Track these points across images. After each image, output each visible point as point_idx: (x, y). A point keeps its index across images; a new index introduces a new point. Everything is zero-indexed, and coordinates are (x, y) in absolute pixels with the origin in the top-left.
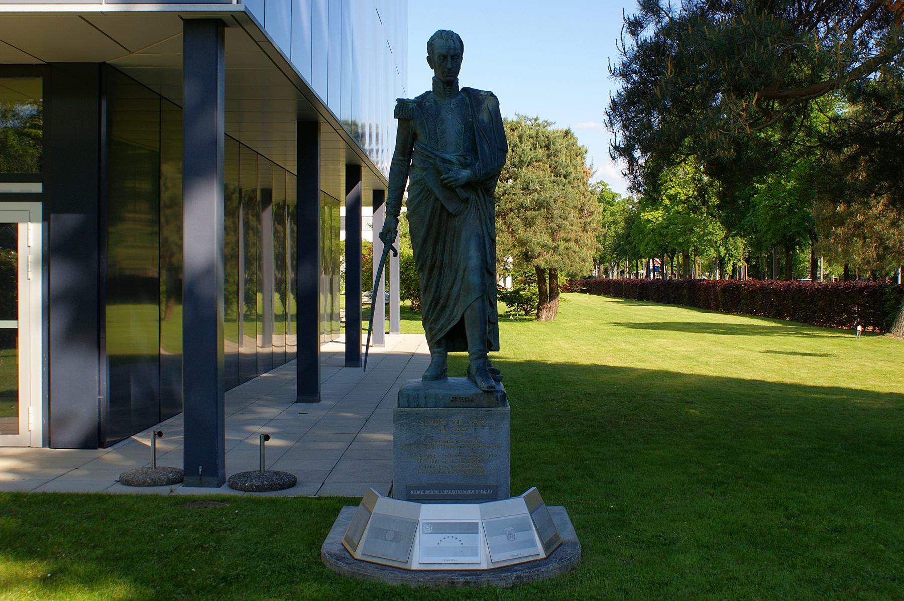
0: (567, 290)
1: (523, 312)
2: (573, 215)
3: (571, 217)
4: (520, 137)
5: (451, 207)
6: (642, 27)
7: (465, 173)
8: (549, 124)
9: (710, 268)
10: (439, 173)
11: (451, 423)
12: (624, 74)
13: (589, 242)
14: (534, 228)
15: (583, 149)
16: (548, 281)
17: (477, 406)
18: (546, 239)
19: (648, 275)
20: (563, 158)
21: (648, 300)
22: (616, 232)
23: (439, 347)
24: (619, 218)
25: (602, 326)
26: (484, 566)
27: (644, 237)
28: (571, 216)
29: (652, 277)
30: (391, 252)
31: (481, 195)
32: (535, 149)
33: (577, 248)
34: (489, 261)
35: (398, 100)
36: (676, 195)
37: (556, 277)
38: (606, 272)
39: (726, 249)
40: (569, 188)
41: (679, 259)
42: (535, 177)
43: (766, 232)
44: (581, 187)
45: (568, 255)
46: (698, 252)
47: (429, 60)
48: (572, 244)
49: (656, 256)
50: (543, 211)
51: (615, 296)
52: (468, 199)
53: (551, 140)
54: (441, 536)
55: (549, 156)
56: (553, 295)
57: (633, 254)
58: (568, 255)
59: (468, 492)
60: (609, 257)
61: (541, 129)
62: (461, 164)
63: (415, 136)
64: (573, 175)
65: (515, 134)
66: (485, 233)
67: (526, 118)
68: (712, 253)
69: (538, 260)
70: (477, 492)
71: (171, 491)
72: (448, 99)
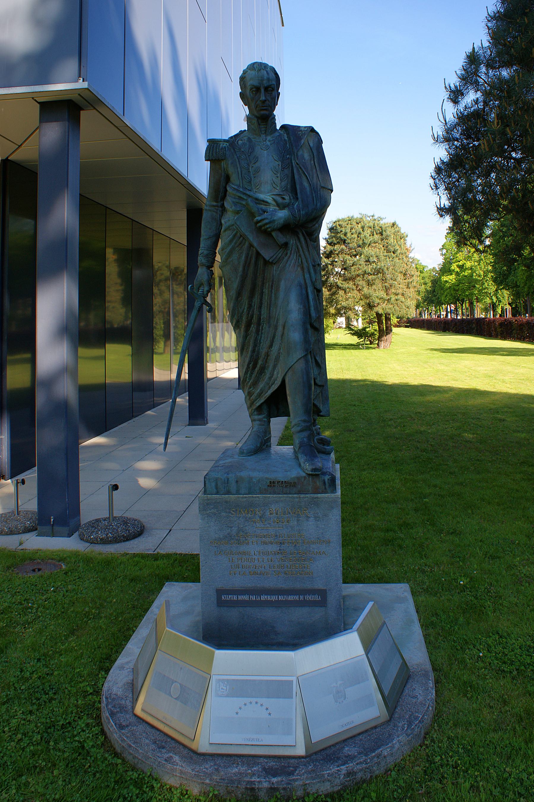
0: (396, 326)
1: (369, 342)
2: (400, 277)
3: (399, 279)
4: (363, 228)
5: (267, 254)
6: (462, 94)
7: (282, 215)
8: (382, 219)
9: (486, 310)
10: (252, 215)
11: (268, 513)
12: (448, 139)
13: (411, 295)
14: (374, 287)
15: (405, 235)
16: (384, 322)
17: (299, 492)
18: (382, 294)
19: (447, 315)
20: (391, 240)
21: (449, 331)
22: (425, 289)
23: (259, 414)
24: (427, 280)
25: (423, 352)
26: (301, 751)
27: (444, 292)
28: (399, 278)
29: (449, 317)
30: (205, 308)
31: (302, 239)
32: (373, 235)
33: (403, 300)
34: (313, 314)
35: (209, 141)
36: (463, 265)
37: (390, 319)
38: (420, 314)
39: (497, 297)
40: (396, 260)
41: (466, 305)
42: (373, 253)
43: (523, 287)
44: (405, 259)
45: (397, 304)
46: (478, 300)
47: (242, 96)
48: (400, 297)
49: (452, 303)
50: (380, 275)
51: (428, 329)
52: (286, 245)
53: (384, 229)
54: (241, 701)
55: (382, 240)
56: (388, 331)
57: (438, 302)
58: (397, 304)
59: (290, 598)
60: (422, 305)
61: (376, 222)
62: (278, 205)
63: (228, 179)
64: (399, 251)
65: (359, 226)
66: (308, 281)
67: (366, 216)
68: (488, 301)
69: (377, 308)
70: (302, 598)
71: (21, 544)
72: (263, 136)
